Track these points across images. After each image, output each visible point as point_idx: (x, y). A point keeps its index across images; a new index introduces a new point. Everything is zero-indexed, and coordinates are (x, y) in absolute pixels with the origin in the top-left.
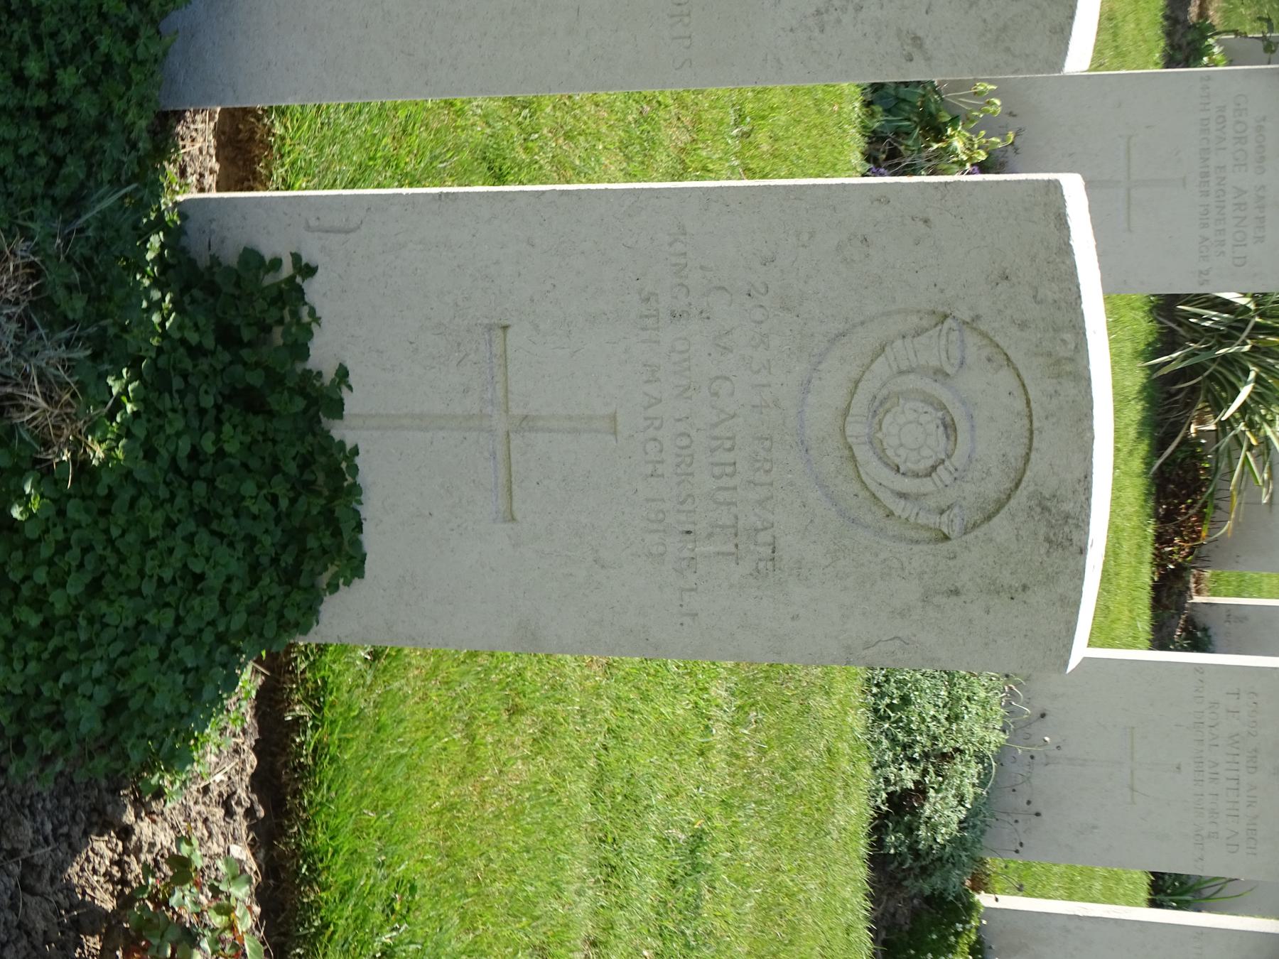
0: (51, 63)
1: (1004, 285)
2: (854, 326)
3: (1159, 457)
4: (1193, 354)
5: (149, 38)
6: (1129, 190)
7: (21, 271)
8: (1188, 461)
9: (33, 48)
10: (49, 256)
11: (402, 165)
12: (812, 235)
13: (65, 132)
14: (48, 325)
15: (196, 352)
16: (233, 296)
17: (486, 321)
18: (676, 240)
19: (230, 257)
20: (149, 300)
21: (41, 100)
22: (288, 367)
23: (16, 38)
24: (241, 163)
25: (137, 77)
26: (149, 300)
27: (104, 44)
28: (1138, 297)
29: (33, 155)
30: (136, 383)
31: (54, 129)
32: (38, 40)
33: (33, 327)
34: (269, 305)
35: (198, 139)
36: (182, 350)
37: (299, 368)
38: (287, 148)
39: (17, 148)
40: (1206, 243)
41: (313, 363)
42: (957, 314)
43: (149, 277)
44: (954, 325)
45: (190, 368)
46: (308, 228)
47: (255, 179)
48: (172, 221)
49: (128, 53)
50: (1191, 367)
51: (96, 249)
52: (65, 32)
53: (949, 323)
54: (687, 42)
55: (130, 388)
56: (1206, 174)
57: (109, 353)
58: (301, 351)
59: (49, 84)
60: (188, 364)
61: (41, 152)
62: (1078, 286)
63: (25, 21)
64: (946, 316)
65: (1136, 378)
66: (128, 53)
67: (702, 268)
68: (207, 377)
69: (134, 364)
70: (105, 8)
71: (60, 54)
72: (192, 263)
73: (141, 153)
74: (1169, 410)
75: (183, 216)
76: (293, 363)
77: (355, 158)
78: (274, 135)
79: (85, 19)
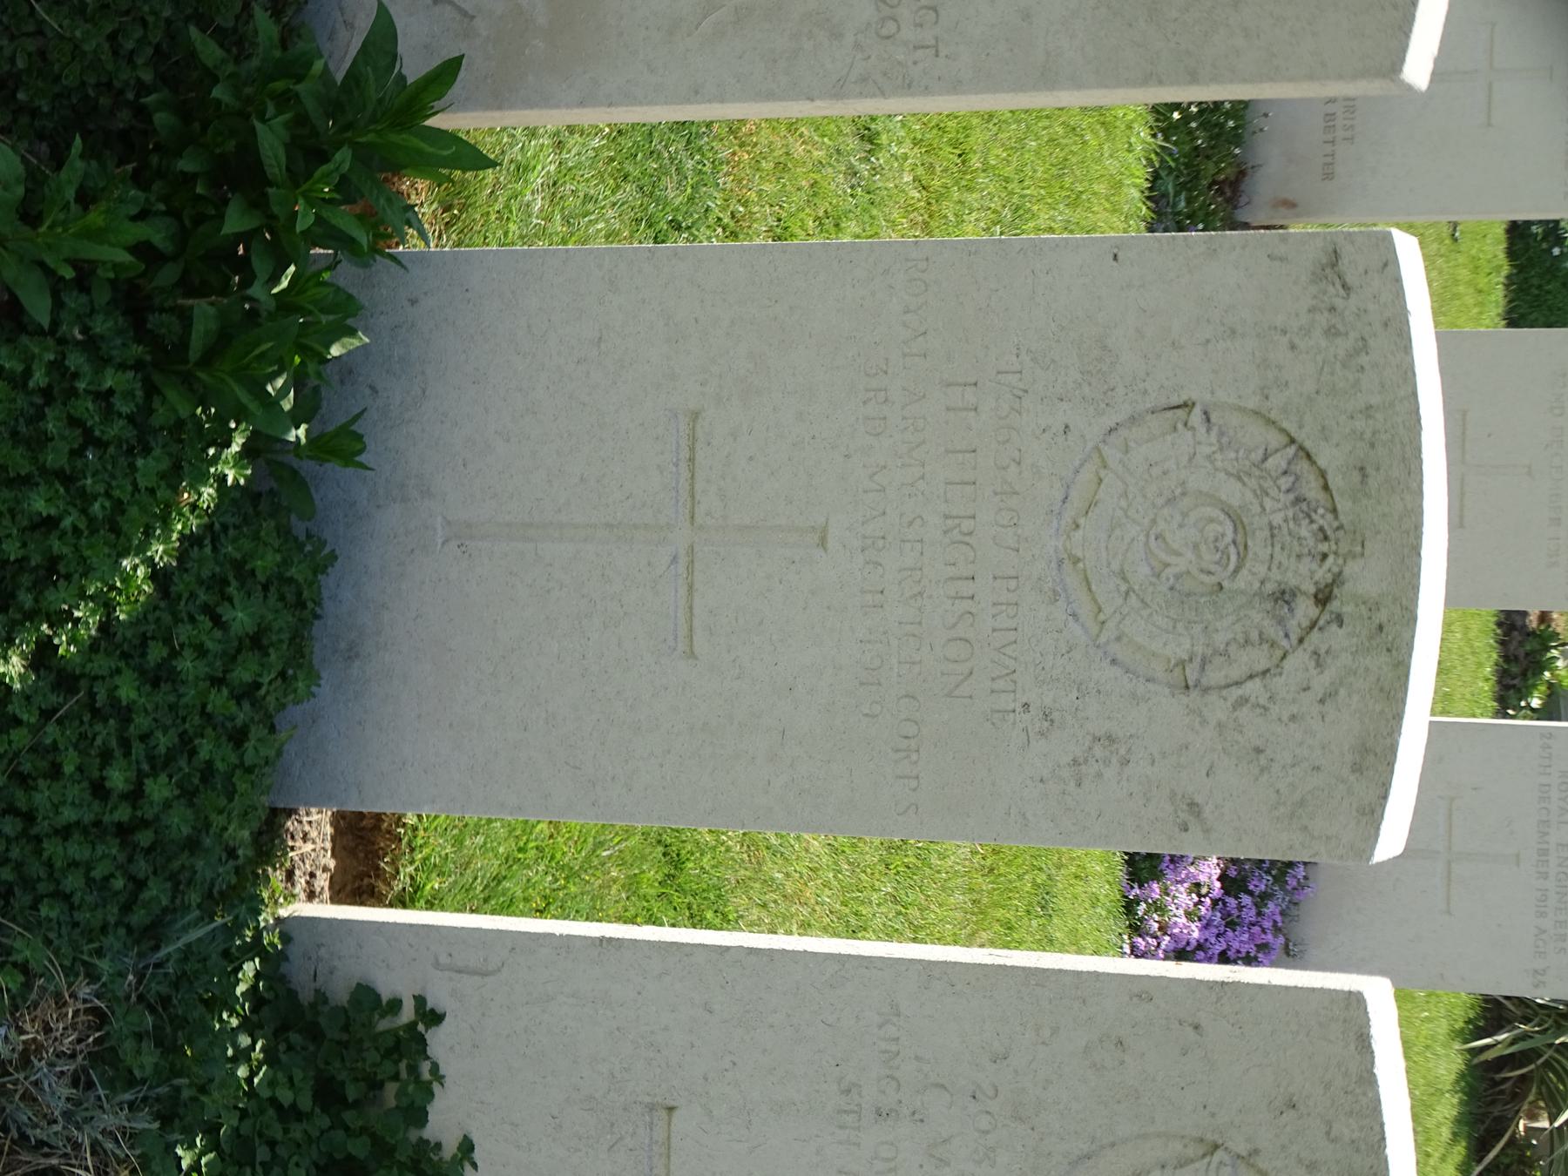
0: (139, 771)
1: (1290, 1115)
2: (1102, 1147)
3: (1479, 1161)
4: (1525, 1037)
5: (259, 740)
6: (1449, 863)
7: (82, 1018)
8: (1514, 1167)
9: (118, 753)
10: (117, 999)
11: (558, 856)
12: (1055, 1031)
13: (149, 851)
14: (110, 1084)
15: (289, 1114)
16: (339, 1043)
17: (647, 1099)
18: (887, 1022)
19: (340, 993)
20: (235, 1046)
21: (123, 814)
22: (401, 1135)
23: (99, 741)
24: (362, 855)
25: (242, 786)
26: (235, 1046)
27: (205, 749)
28: (1457, 1005)
29: (106, 879)
30: (212, 1155)
31: (136, 846)
32: (125, 744)
33: (90, 1085)
34: (383, 1057)
35: (312, 839)
36: (271, 1112)
37: (413, 1135)
38: (420, 841)
39: (89, 869)
40: (1544, 936)
41: (431, 1132)
42: (1229, 1144)
43: (238, 1015)
44: (1227, 1158)
45: (279, 1136)
46: (437, 965)
47: (377, 876)
48: (272, 944)
49: (234, 759)
50: (1522, 1052)
51: (176, 986)
52: (159, 734)
53: (1219, 1155)
54: (914, 783)
55: (203, 1161)
56: (1544, 852)
57: (181, 1119)
58: (418, 1116)
59: (136, 795)
60: (277, 1132)
61: (118, 874)
62: (1382, 1125)
63: (112, 722)
64: (1216, 1147)
65: (1449, 1064)
66: (234, 759)
67: (917, 1058)
68: (299, 1146)
69: (211, 1130)
70: (209, 708)
71: (151, 759)
72: (292, 994)
73: (241, 861)
74: (1493, 1102)
75: (286, 938)
76: (406, 1130)
77: (501, 850)
78: (404, 825)
79: (184, 720)
